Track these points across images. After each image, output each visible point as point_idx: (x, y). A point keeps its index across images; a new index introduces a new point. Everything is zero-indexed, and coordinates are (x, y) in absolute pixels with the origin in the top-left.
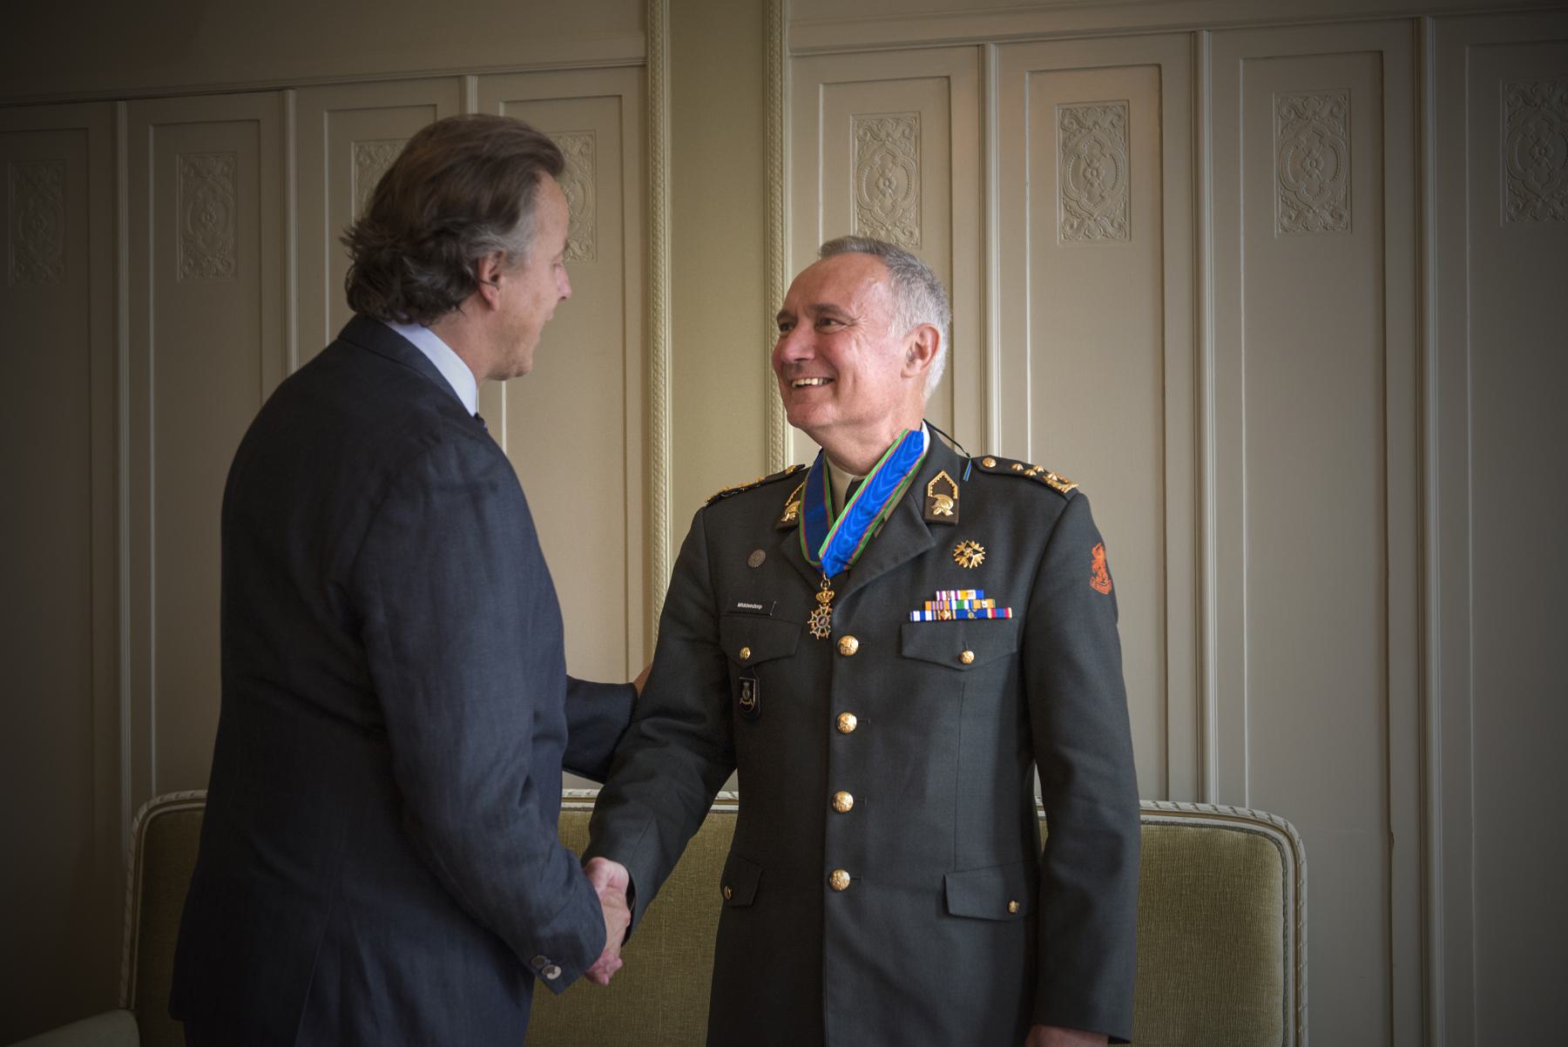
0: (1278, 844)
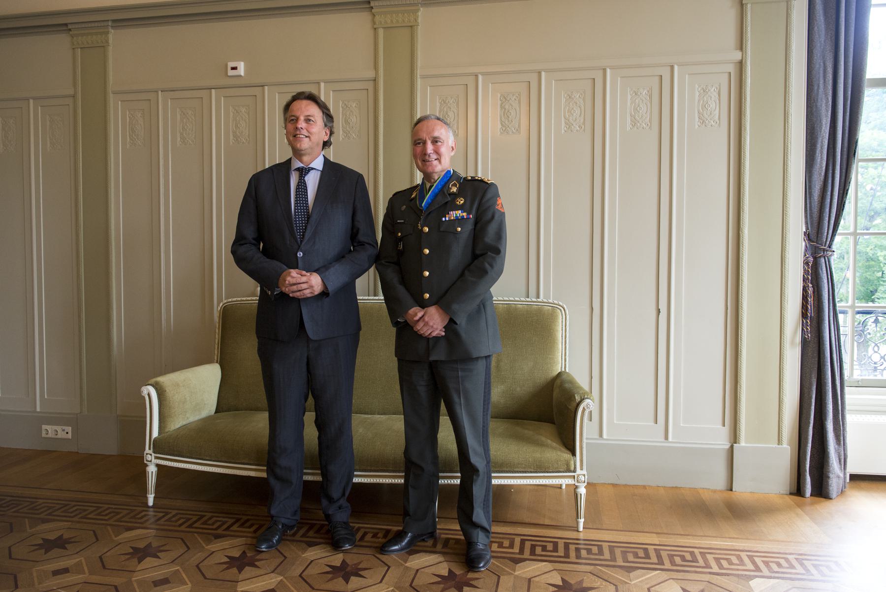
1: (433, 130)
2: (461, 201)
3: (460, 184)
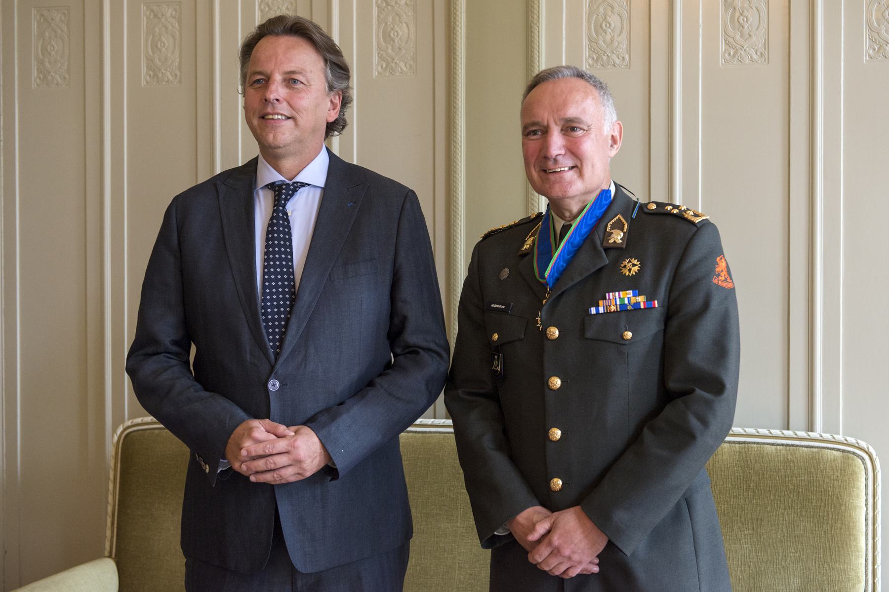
0: (863, 459)
1: (565, 104)
2: (632, 267)
3: (632, 222)
